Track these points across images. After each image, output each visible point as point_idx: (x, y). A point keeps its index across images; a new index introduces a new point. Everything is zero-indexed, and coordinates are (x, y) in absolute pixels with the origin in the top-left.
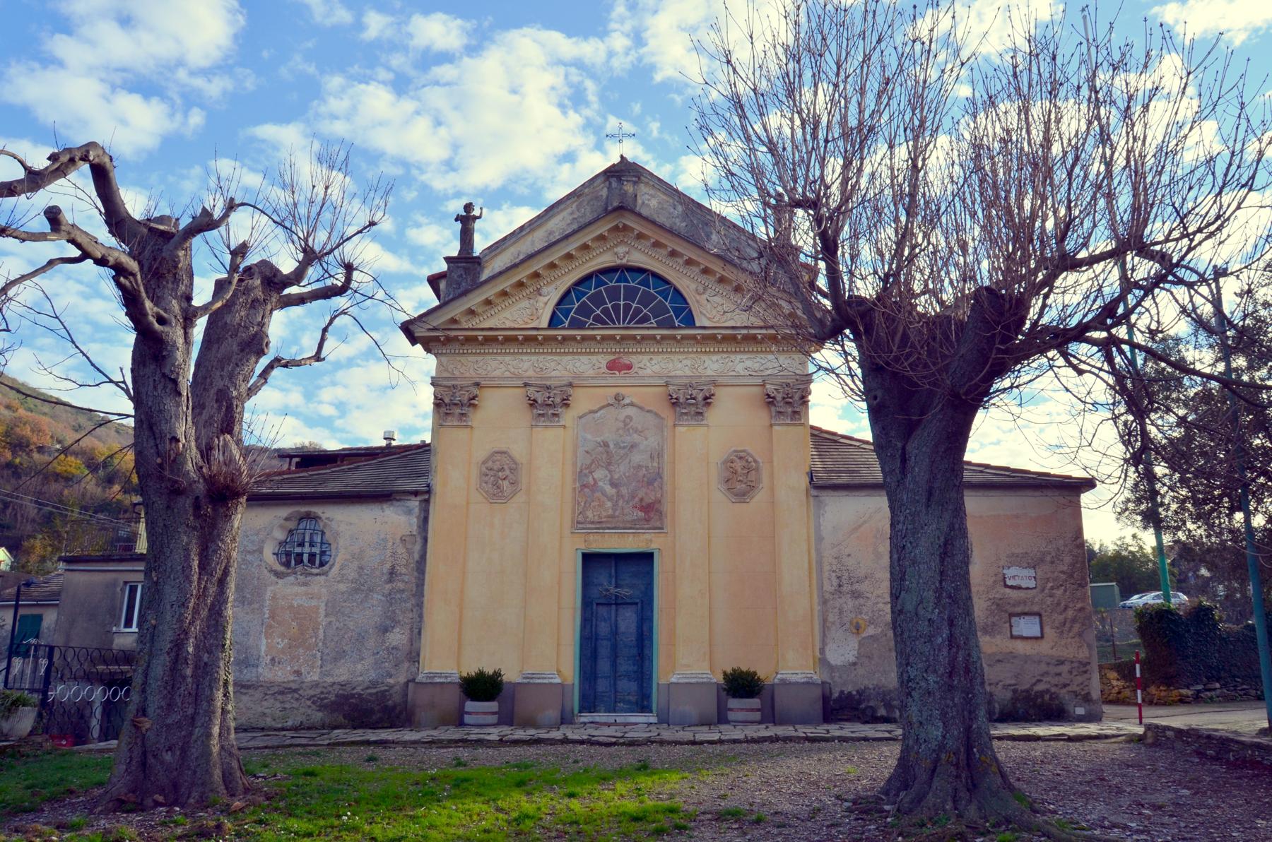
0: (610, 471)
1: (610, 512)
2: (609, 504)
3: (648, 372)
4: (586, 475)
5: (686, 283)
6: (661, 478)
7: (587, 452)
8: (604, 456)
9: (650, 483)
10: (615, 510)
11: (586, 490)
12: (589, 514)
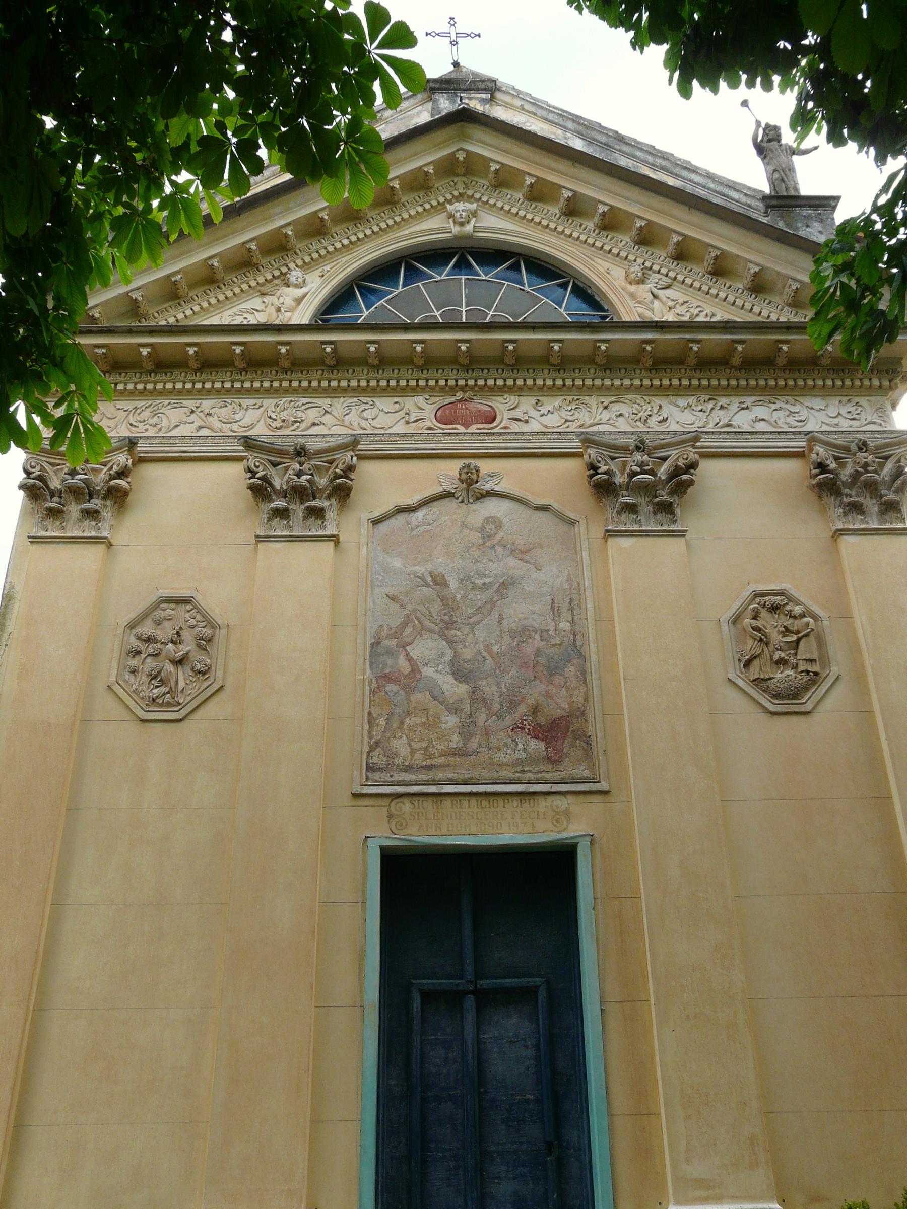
0: (451, 643)
1: (455, 741)
2: (451, 721)
3: (534, 426)
4: (389, 652)
6: (582, 656)
7: (393, 599)
8: (436, 607)
9: (553, 670)
10: (466, 737)
11: (390, 687)
12: (401, 746)
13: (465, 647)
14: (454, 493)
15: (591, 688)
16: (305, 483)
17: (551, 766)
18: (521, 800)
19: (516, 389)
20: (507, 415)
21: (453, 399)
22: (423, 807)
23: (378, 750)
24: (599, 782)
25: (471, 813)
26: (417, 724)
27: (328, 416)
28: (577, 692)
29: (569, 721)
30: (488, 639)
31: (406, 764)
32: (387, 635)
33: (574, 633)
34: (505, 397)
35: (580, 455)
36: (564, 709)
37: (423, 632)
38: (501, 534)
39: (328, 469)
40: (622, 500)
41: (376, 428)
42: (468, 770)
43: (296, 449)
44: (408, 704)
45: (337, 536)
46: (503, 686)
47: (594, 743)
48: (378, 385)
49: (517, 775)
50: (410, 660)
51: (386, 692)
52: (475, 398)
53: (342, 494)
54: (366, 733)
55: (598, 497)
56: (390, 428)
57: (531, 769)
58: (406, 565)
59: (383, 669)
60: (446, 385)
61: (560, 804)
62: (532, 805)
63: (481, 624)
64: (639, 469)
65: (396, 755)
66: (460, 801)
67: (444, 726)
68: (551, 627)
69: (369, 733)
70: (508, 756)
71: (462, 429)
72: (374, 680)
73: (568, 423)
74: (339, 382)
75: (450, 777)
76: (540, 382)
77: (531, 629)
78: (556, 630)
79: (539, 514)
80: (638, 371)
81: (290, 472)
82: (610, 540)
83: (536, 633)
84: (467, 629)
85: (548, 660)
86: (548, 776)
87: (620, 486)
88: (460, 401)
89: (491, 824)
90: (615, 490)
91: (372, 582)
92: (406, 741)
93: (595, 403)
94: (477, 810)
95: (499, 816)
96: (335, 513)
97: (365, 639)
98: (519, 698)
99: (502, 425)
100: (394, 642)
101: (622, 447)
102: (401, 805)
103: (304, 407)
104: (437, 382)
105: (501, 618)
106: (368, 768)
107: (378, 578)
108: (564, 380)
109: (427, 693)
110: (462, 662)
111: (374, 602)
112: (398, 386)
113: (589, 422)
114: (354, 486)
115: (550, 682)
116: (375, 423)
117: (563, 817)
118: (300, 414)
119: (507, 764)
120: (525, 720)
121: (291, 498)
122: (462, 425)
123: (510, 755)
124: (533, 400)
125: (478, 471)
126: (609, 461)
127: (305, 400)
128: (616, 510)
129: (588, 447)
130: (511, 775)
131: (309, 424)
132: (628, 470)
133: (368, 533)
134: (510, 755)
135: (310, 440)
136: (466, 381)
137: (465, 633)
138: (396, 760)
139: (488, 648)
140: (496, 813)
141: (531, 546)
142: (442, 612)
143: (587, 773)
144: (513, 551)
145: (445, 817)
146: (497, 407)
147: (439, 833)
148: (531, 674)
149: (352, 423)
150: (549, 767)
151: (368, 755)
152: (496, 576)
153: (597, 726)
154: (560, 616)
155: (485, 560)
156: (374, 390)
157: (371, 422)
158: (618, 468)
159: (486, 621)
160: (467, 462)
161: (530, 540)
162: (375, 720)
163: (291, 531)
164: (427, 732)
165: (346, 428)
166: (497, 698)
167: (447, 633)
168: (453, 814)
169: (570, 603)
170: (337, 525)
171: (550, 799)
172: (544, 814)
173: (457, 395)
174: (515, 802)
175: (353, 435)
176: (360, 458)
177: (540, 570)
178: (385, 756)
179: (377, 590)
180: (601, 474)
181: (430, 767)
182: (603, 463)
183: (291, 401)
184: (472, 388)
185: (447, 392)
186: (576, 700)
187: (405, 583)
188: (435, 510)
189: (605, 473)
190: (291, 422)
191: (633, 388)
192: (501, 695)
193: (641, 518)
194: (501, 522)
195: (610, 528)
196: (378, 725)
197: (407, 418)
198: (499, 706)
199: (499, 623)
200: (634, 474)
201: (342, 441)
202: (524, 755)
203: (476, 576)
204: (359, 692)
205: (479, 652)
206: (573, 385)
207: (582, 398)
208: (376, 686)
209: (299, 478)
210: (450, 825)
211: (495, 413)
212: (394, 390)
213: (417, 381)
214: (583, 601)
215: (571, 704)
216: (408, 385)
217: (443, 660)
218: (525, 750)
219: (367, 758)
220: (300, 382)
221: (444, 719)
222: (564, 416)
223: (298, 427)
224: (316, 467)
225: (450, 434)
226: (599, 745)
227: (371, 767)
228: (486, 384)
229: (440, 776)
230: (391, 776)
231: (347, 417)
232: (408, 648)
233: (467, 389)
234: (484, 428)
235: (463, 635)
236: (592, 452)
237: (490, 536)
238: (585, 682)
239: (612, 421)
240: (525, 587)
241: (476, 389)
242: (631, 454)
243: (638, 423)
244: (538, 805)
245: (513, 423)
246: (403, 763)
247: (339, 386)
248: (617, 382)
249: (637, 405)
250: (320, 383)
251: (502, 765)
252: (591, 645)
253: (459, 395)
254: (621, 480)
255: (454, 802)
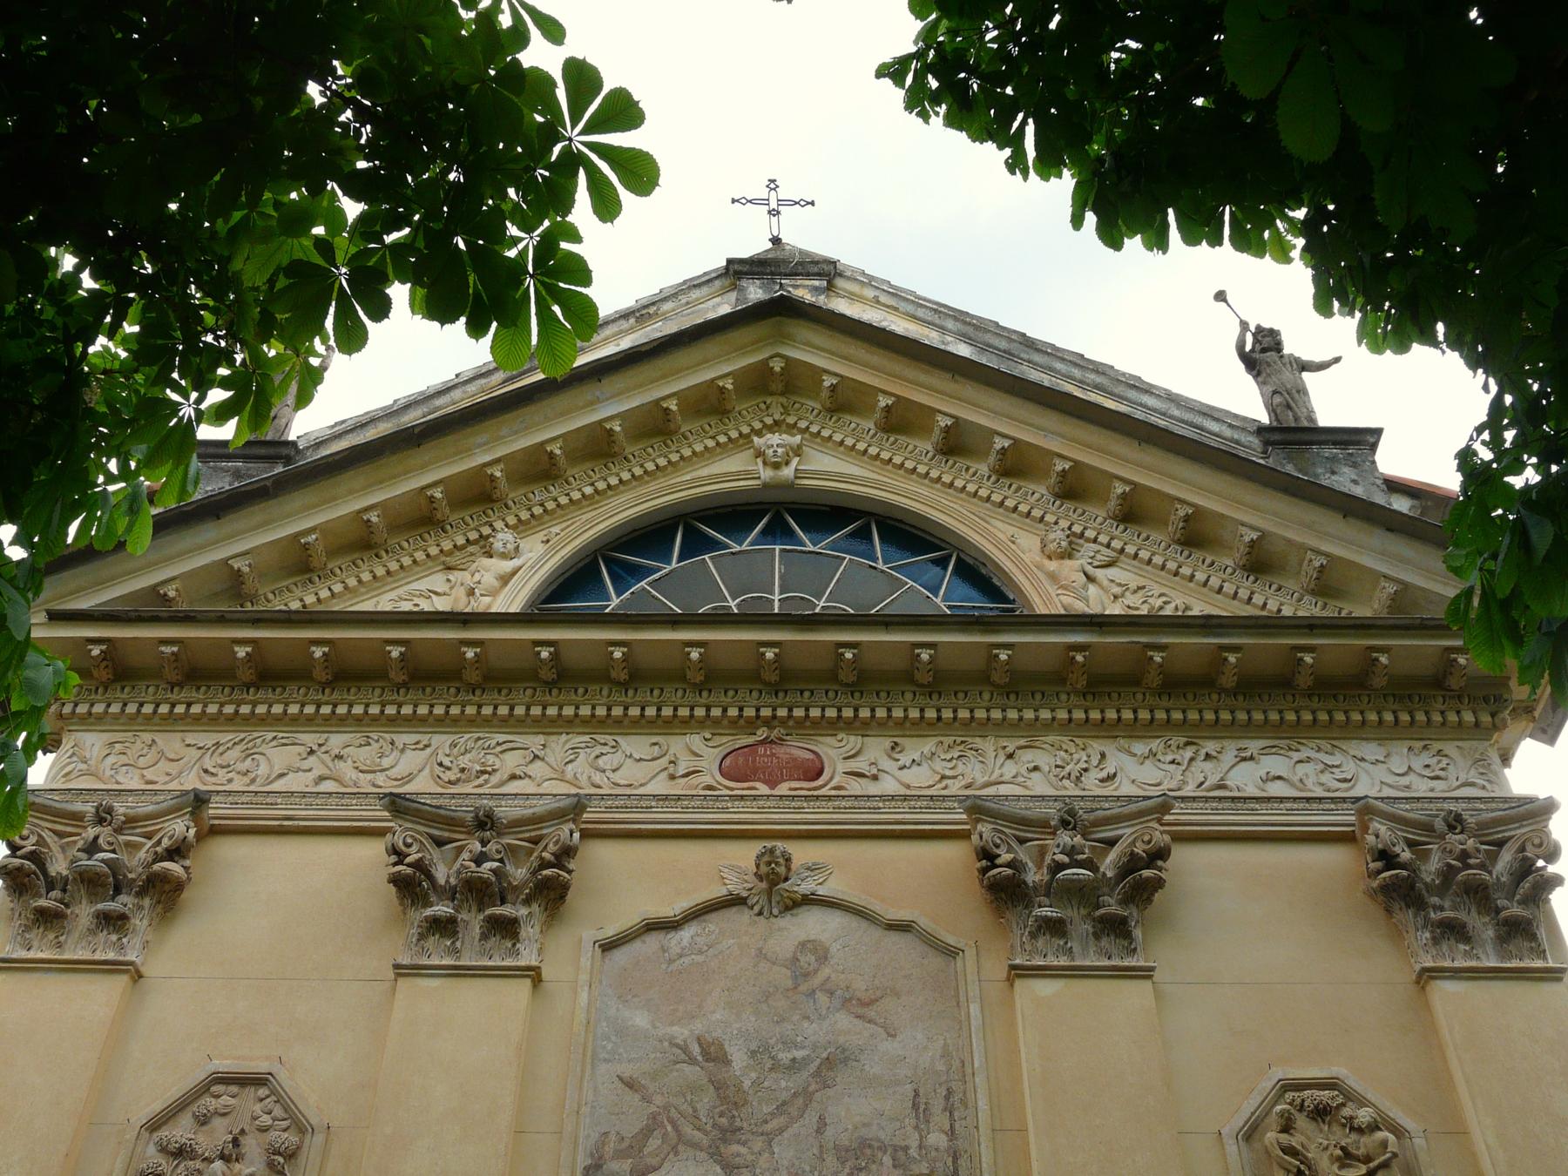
3: (888, 786)
5: (1281, 1154)
7: (630, 1084)
8: (706, 1101)
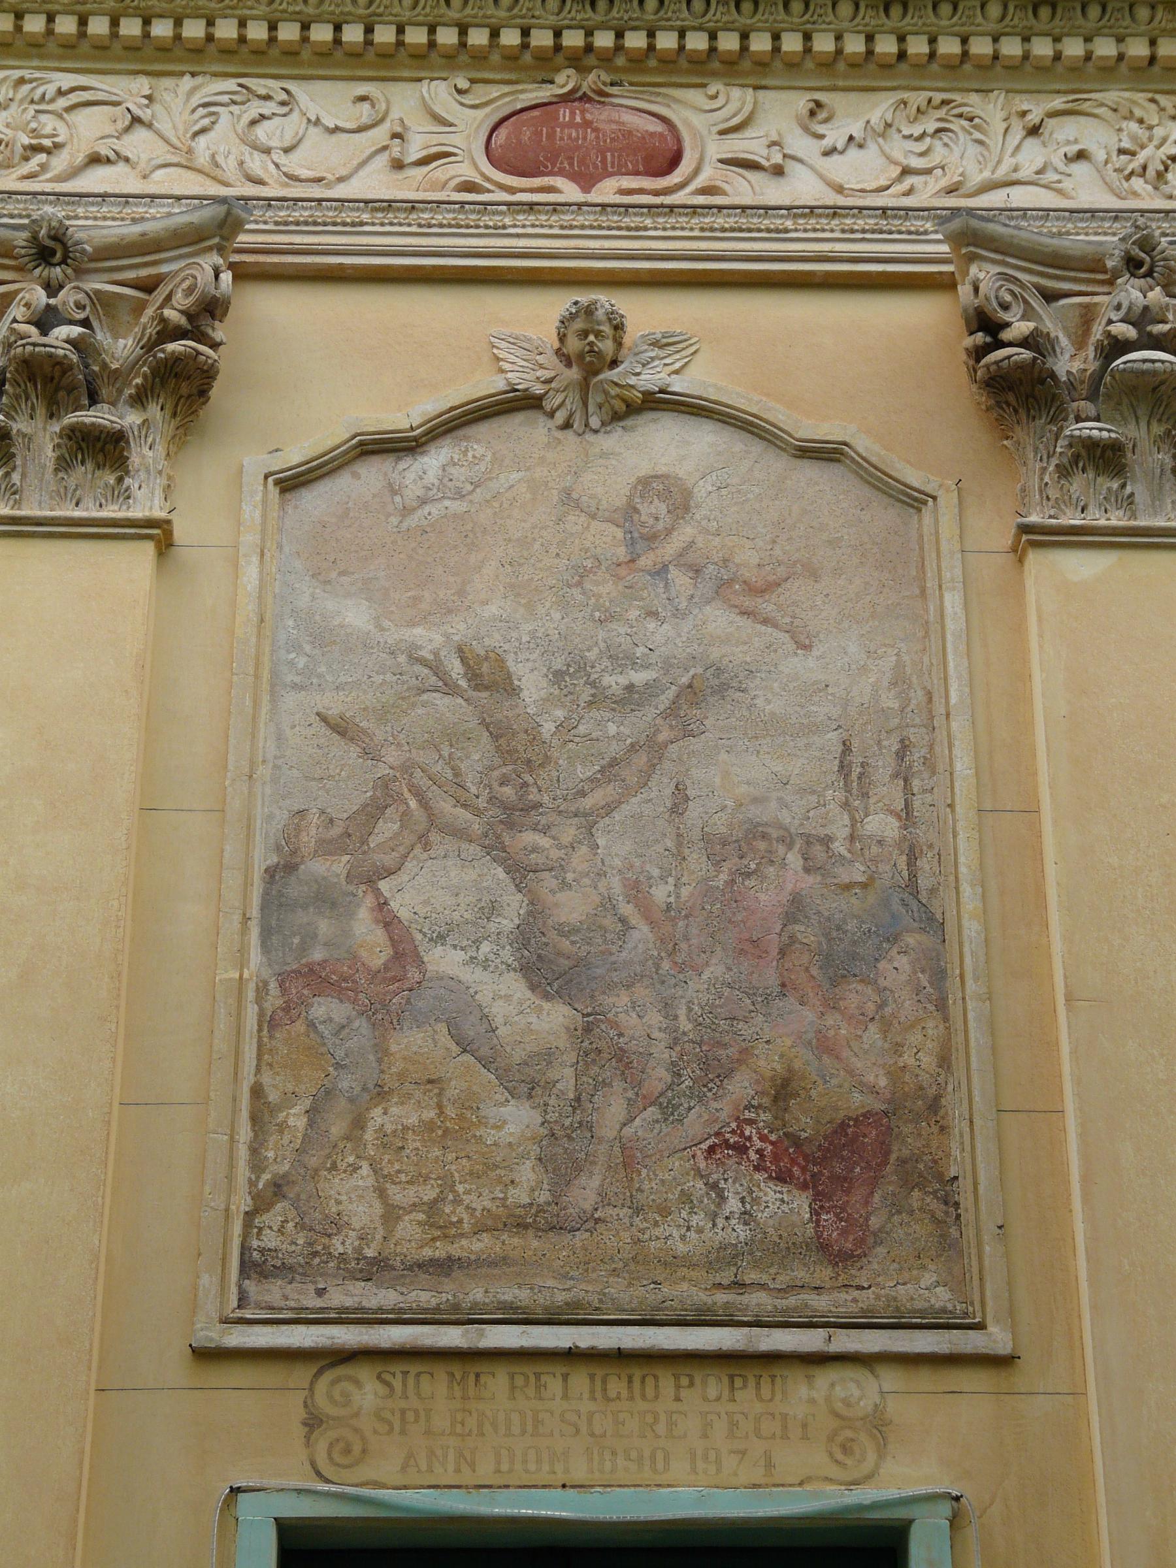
6: (934, 924)
7: (340, 728)
11: (326, 1009)
13: (565, 885)
14: (540, 398)
15: (959, 1024)
16: (64, 352)
17: (829, 1272)
18: (731, 1378)
19: (746, 64)
20: (717, 149)
21: (543, 93)
22: (418, 1394)
23: (279, 1207)
24: (980, 1326)
25: (573, 1418)
26: (405, 1128)
27: (141, 133)
28: (915, 1038)
29: (889, 1128)
30: (637, 862)
31: (370, 1253)
32: (321, 842)
33: (912, 848)
34: (712, 90)
35: (944, 284)
36: (873, 1090)
37: (434, 837)
38: (686, 532)
39: (139, 308)
40: (1075, 429)
41: (297, 179)
42: (566, 1276)
43: (35, 238)
44: (380, 1061)
45: (164, 525)
46: (682, 1012)
47: (966, 1200)
48: (305, 39)
49: (721, 1297)
50: (387, 920)
51: (311, 1025)
52: (614, 90)
53: (185, 389)
54: (243, 1152)
55: (1000, 420)
56: (341, 180)
57: (765, 1278)
58: (386, 623)
59: (303, 949)
60: (525, 46)
61: (856, 1393)
62: (766, 1392)
63: (617, 816)
64: (1130, 332)
65: (337, 1224)
66: (538, 1376)
67: (490, 1138)
68: (840, 829)
69: (254, 1151)
70: (692, 1235)
71: (570, 191)
72: (273, 985)
73: (910, 181)
74: (178, 23)
75: (508, 1297)
76: (824, 44)
77: (774, 833)
78: (852, 838)
79: (810, 471)
80: (1143, 13)
81: (17, 311)
82: (1033, 558)
83: (790, 847)
84: (572, 831)
85: (827, 935)
86: (821, 1303)
87: (1071, 385)
88: (566, 99)
89: (634, 1455)
90: (1054, 397)
91: (275, 674)
92: (371, 1181)
93: (1001, 115)
94: (591, 1406)
95: (661, 1428)
96: (160, 449)
97: (248, 855)
98: (732, 1051)
99: (698, 183)
100: (339, 866)
101: (1083, 258)
102: (347, 1386)
103: (62, 103)
104: (495, 34)
105: (680, 799)
106: (247, 1267)
107: (292, 663)
108: (901, 39)
109: (442, 1028)
110: (553, 935)
111: (280, 738)
112: (368, 43)
113: (976, 178)
114: (222, 366)
115: (832, 1005)
116: (294, 163)
117: (863, 1437)
118: (49, 124)
119: (687, 1262)
120: (751, 1122)
121: (17, 397)
122: (574, 177)
123: (700, 1231)
124: (801, 102)
125: (619, 328)
126: (1036, 303)
127: (67, 80)
128: (1055, 461)
129: (972, 258)
130: (703, 1297)
131: (80, 159)
132: (1097, 332)
133: (264, 516)
134: (700, 1231)
135: (80, 211)
136: (589, 33)
137: (566, 839)
138: (336, 1242)
139: (636, 890)
140: (649, 1419)
141: (782, 571)
142: (496, 774)
143: (942, 1297)
144: (722, 587)
145: (487, 1428)
146: (686, 122)
147: (467, 1478)
148: (771, 978)
149: (220, 159)
150: (823, 1274)
151: (248, 1223)
152: (667, 666)
153: (978, 1145)
154: (865, 796)
155: (633, 614)
156: (291, 54)
157: (282, 159)
158: (1065, 328)
159: (632, 805)
160: (584, 297)
161: (778, 552)
162: (273, 1110)
163: (17, 504)
164: (437, 1152)
165: (200, 178)
166: (662, 1053)
167: (507, 840)
168: (515, 1417)
169: (901, 755)
170: (168, 490)
171: (825, 1378)
172: (804, 1426)
173: (560, 78)
174: (714, 1384)
175: (223, 200)
176: (242, 274)
177: (807, 648)
178: (301, 1226)
179: (290, 700)
180: (1010, 344)
181: (444, 1267)
182: (1017, 310)
183: (21, 81)
184: (606, 59)
185: (526, 68)
186: (911, 1061)
187: (378, 679)
188: (479, 449)
189: (1024, 343)
190: (19, 150)
191: (1123, 67)
192: (676, 1041)
193: (1137, 488)
194: (687, 494)
195: (1034, 518)
196: (282, 1127)
197: (396, 151)
198: (668, 1078)
199: (676, 811)
200: (1116, 347)
201: (187, 218)
202: (743, 1232)
203: (606, 662)
204: (223, 1025)
205: (608, 904)
206: (932, 55)
207: (957, 97)
208: (279, 1002)
209: (44, 333)
210: (504, 1452)
211: (679, 140)
212: (355, 55)
213: (432, 30)
214: (941, 750)
215: (896, 1074)
216: (400, 43)
217: (492, 927)
218: (746, 1217)
219: (245, 1236)
220: (51, 19)
221: (490, 1112)
222: (897, 155)
223: (44, 167)
224: (101, 301)
225: (531, 207)
226: (983, 1207)
227: (255, 1265)
228: (651, 47)
229: (477, 1294)
230: (321, 1292)
231: (202, 140)
232: (383, 885)
233: (591, 60)
234: (641, 191)
235: (560, 847)
236: (985, 273)
237: (651, 538)
238: (941, 1005)
239: (1051, 176)
240: (759, 702)
241: (620, 61)
242: (1111, 282)
243: (1137, 183)
244: (784, 1393)
245: (733, 173)
246: (358, 1250)
247: (178, 37)
248: (1074, 48)
249: (1133, 126)
250: (115, 23)
251: (673, 1263)
252: (966, 890)
253: (566, 80)
254: (1076, 366)
255: (520, 1381)
